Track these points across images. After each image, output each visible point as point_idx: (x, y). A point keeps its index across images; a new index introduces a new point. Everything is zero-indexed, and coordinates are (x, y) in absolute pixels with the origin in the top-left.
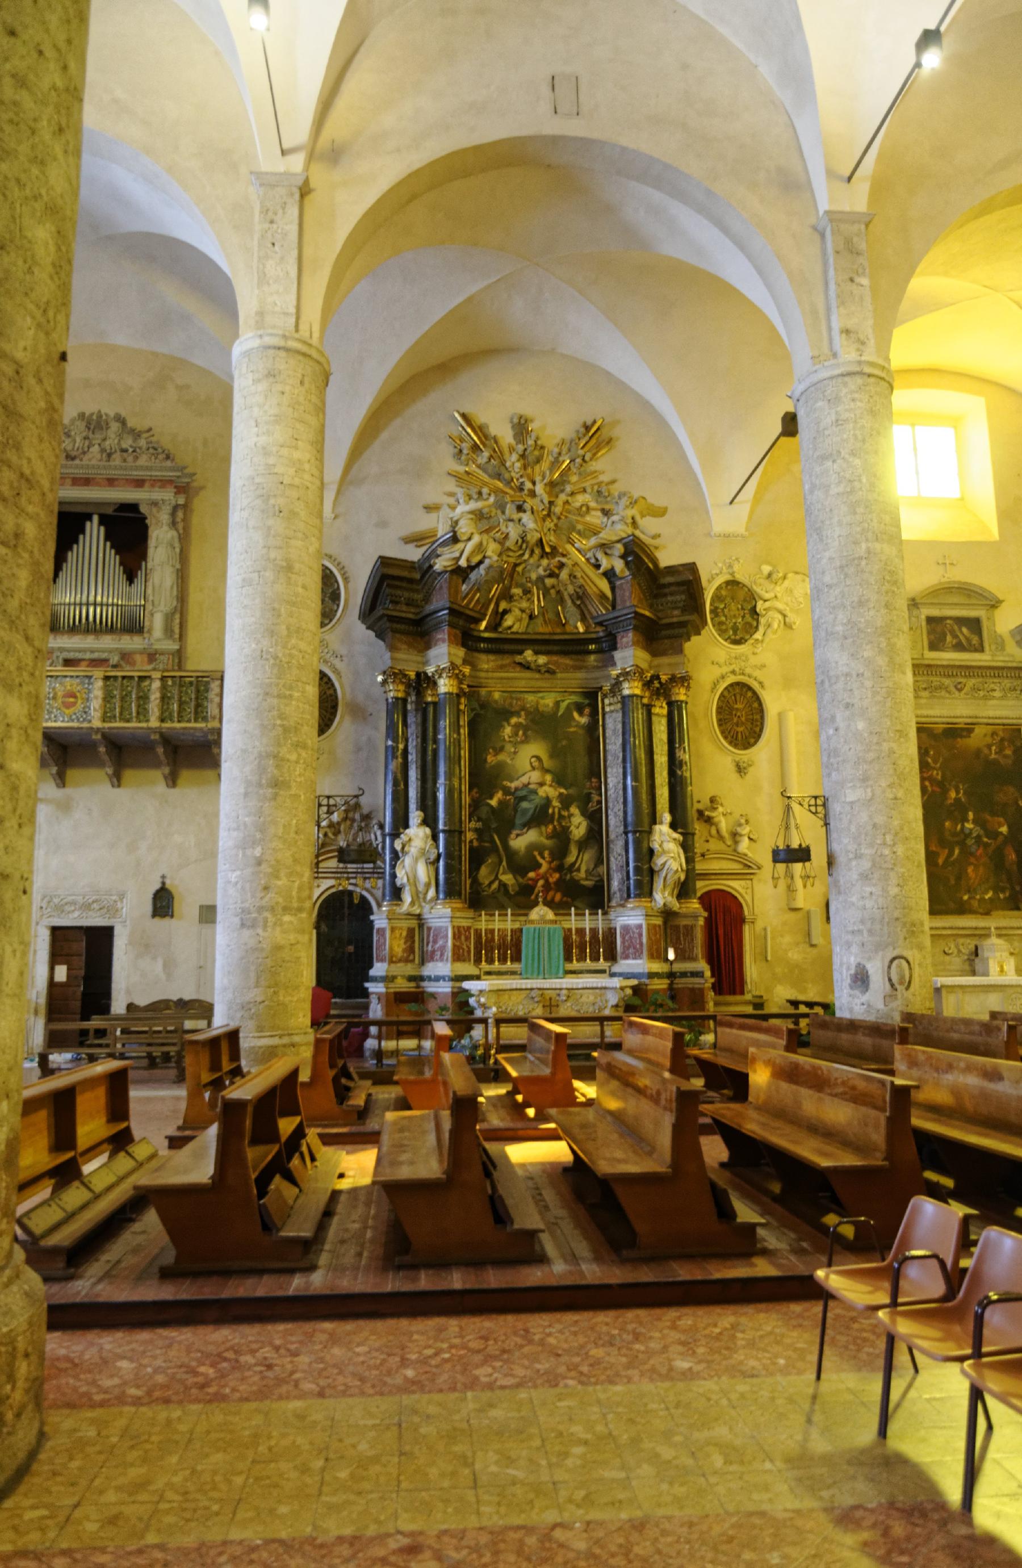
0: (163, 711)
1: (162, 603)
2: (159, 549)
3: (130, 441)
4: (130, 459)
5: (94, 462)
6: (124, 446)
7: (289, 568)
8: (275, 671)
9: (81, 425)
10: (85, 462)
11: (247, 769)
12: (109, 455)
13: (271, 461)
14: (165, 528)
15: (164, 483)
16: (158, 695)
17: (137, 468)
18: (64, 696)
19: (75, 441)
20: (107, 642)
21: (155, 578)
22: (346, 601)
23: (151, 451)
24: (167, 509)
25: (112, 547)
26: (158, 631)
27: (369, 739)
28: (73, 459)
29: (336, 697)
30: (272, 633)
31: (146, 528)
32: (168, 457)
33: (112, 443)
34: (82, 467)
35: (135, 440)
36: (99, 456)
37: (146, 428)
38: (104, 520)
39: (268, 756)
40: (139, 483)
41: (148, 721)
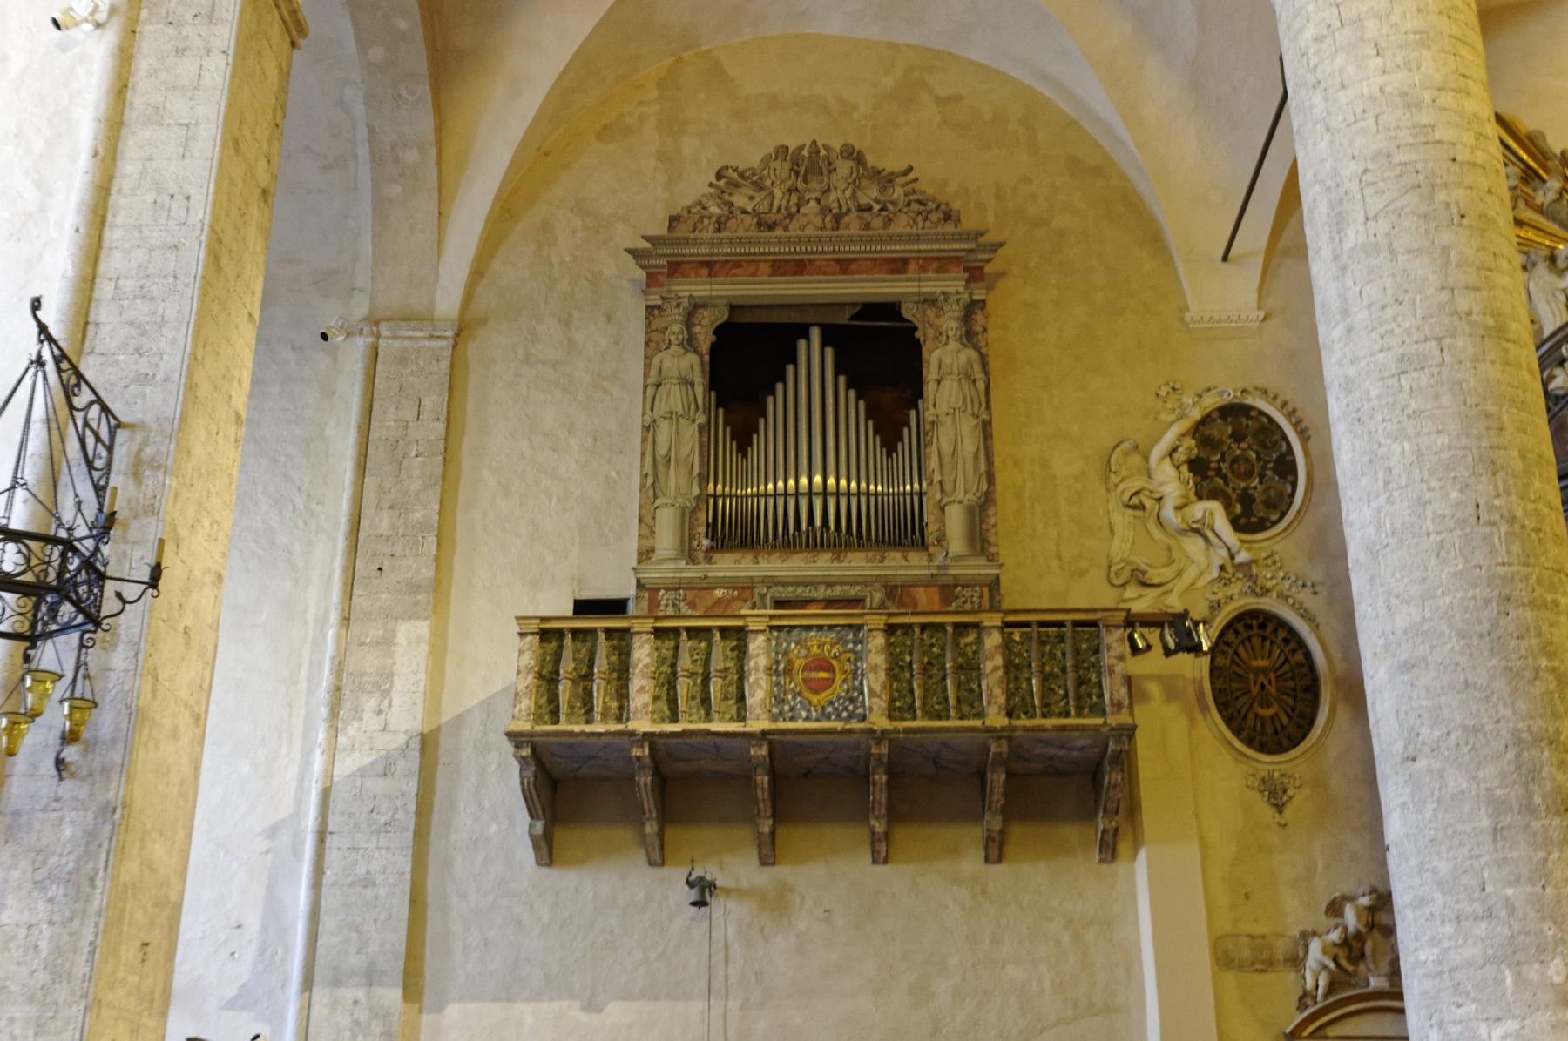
0: (1010, 695)
3: (874, 192)
4: (877, 222)
5: (810, 231)
6: (864, 200)
7: (1499, 331)
8: (1516, 548)
9: (783, 168)
10: (794, 231)
11: (1489, 771)
12: (837, 219)
13: (1425, 118)
14: (953, 345)
15: (943, 263)
16: (999, 661)
17: (891, 239)
18: (806, 668)
20: (858, 564)
21: (943, 438)
23: (915, 206)
24: (953, 311)
28: (771, 227)
29: (1312, 668)
30: (1494, 468)
31: (916, 347)
32: (948, 217)
33: (839, 195)
34: (789, 240)
35: (883, 190)
36: (818, 221)
37: (904, 167)
38: (831, 336)
39: (1537, 740)
40: (898, 266)
41: (980, 715)
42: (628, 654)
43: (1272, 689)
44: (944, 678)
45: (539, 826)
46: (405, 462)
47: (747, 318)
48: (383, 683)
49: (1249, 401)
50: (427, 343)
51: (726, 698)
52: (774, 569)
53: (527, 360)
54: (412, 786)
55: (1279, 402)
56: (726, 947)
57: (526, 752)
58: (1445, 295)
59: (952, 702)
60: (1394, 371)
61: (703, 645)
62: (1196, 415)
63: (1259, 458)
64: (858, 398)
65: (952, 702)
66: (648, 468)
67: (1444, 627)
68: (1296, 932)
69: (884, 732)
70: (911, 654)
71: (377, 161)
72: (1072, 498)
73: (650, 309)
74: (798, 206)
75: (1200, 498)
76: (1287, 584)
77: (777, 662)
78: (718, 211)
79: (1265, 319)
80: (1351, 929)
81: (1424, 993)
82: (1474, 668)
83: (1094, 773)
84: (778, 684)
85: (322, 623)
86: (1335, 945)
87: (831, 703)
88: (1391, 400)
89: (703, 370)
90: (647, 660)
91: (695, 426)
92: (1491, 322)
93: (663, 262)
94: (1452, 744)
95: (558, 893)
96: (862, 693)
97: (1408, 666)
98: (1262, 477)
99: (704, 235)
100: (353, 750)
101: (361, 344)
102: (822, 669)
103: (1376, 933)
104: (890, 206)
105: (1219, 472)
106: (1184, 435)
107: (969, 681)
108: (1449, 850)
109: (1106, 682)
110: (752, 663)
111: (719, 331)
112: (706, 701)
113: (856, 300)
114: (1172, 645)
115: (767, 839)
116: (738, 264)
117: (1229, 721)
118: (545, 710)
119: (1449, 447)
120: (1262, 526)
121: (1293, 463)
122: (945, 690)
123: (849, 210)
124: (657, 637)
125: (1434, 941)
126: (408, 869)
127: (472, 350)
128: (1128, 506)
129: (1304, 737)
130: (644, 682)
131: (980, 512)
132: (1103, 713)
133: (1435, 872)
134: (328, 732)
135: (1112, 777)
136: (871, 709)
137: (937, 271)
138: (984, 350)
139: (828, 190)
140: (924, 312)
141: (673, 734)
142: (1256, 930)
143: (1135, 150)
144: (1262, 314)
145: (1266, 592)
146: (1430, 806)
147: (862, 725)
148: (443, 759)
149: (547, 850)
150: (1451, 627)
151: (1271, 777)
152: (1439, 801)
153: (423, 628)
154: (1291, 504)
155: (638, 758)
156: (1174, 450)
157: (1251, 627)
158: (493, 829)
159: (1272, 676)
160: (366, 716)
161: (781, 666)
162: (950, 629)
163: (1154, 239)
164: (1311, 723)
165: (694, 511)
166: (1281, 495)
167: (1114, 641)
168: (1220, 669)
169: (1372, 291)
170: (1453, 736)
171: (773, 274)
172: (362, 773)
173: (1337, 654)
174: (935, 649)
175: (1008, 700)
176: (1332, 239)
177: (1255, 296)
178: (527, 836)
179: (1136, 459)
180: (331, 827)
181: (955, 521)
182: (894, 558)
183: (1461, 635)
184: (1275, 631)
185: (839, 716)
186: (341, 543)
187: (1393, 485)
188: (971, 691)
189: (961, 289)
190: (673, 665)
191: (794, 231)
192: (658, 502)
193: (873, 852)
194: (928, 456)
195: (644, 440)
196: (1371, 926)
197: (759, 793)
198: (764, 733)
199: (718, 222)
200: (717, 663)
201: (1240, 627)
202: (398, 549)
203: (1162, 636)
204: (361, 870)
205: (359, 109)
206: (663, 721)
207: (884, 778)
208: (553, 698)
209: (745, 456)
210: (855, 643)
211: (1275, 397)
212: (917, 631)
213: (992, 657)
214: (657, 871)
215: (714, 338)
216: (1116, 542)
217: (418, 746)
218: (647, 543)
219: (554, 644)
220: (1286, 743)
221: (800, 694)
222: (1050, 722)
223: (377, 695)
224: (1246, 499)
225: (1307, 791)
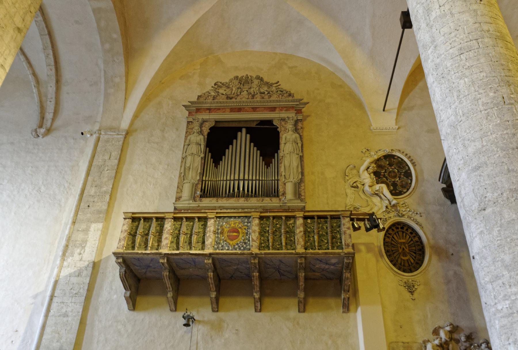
1: (292, 177)
2: (288, 145)
3: (266, 89)
4: (266, 97)
5: (244, 99)
6: (262, 91)
9: (236, 82)
12: (253, 96)
14: (291, 132)
15: (288, 108)
16: (302, 229)
17: (271, 102)
18: (229, 232)
19: (232, 90)
22: (417, 177)
23: (279, 92)
25: (254, 146)
26: (290, 194)
27: (455, 273)
28: (231, 98)
29: (422, 242)
31: (278, 133)
33: (254, 88)
35: (269, 88)
36: (247, 97)
37: (276, 81)
38: (249, 130)
40: (273, 109)
42: (163, 227)
43: (407, 250)
44: (281, 236)
45: (128, 293)
46: (103, 172)
47: (221, 125)
48: (83, 244)
49: (394, 153)
50: (116, 136)
51: (198, 242)
52: (224, 203)
53: (149, 142)
54: (87, 280)
55: (404, 154)
56: (197, 343)
57: (120, 260)
58: (477, 25)
59: (284, 244)
60: (457, 54)
61: (192, 223)
62: (376, 157)
63: (398, 171)
64: (257, 150)
65: (284, 244)
66: (182, 171)
67: (494, 148)
68: (421, 341)
69: (256, 254)
70: (269, 227)
71: (106, 82)
72: (330, 175)
73: (188, 122)
74: (240, 93)
75: (377, 183)
76: (410, 213)
77: (218, 229)
78: (214, 94)
79: (398, 129)
80: (443, 340)
81: (502, 327)
82: (512, 163)
83: (340, 279)
84: (218, 237)
85: (66, 224)
86: (437, 346)
87: (237, 244)
88: (457, 65)
89: (204, 140)
90: (169, 228)
91: (200, 158)
92: (499, 34)
93: (194, 108)
94: (505, 199)
95: (135, 321)
96: (249, 241)
97: (477, 168)
98: (400, 177)
99: (209, 101)
100: (68, 267)
101: (95, 136)
102: (234, 232)
103: (453, 342)
104: (271, 92)
105: (384, 176)
106: (372, 163)
107: (290, 237)
108: (509, 248)
109: (343, 237)
110: (208, 229)
111: (211, 129)
112: (190, 243)
113: (258, 119)
114: (368, 226)
115: (214, 300)
116: (219, 109)
117: (391, 261)
118: (130, 246)
119: (486, 77)
120: (400, 193)
121: (411, 173)
122: (281, 240)
123: (257, 93)
124: (174, 221)
125: (506, 297)
126: (81, 311)
127: (131, 139)
128: (352, 187)
129: (421, 266)
130: (167, 236)
131: (298, 186)
132: (342, 249)
133: (503, 261)
134: (61, 260)
135: (347, 275)
136: (252, 246)
137: (286, 111)
138: (301, 134)
139: (251, 88)
140: (281, 123)
141: (176, 254)
142: (405, 340)
143: (353, 77)
144: (397, 127)
145: (403, 216)
146: (496, 229)
147: (249, 252)
148: (101, 271)
149: (133, 303)
150: (497, 147)
151: (408, 281)
152: (501, 226)
153: (100, 226)
154: (410, 186)
155: (163, 264)
156: (368, 168)
157: (398, 228)
158: (115, 296)
159: (407, 245)
160: (75, 255)
161: (219, 231)
162: (284, 218)
163: (360, 105)
164: (422, 261)
165: (197, 185)
166: (407, 183)
167: (346, 223)
168: (387, 242)
169: (445, 30)
170: (505, 195)
171: (231, 112)
172: (70, 275)
173: (430, 237)
174: (278, 226)
175: (305, 244)
176: (426, 19)
177: (395, 122)
178: (124, 298)
179: (355, 172)
180: (56, 295)
181: (289, 189)
182: (267, 200)
183: (503, 149)
184: (407, 230)
185: (240, 249)
186: (77, 197)
187: (461, 96)
188: (291, 240)
189: (294, 116)
190: (179, 231)
191: (238, 99)
192: (185, 181)
193: (255, 306)
194: (281, 167)
195: (182, 162)
196: (451, 339)
197: (210, 280)
198: (210, 254)
199: (214, 97)
200: (195, 230)
201: (394, 228)
202: (96, 200)
203: (365, 224)
204: (64, 311)
205: (102, 66)
206: (174, 250)
207: (257, 274)
208: (134, 242)
209: (217, 168)
210: (248, 223)
211: (403, 153)
212: (271, 218)
213: (299, 228)
214: (174, 314)
215: (209, 131)
216: (348, 199)
217: (92, 266)
218: (179, 195)
219: (137, 223)
220: (413, 269)
221: (226, 241)
222: (320, 251)
223: (80, 248)
224: (394, 185)
225: (422, 287)
